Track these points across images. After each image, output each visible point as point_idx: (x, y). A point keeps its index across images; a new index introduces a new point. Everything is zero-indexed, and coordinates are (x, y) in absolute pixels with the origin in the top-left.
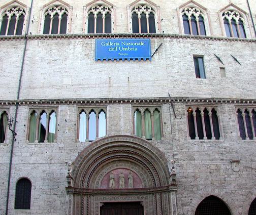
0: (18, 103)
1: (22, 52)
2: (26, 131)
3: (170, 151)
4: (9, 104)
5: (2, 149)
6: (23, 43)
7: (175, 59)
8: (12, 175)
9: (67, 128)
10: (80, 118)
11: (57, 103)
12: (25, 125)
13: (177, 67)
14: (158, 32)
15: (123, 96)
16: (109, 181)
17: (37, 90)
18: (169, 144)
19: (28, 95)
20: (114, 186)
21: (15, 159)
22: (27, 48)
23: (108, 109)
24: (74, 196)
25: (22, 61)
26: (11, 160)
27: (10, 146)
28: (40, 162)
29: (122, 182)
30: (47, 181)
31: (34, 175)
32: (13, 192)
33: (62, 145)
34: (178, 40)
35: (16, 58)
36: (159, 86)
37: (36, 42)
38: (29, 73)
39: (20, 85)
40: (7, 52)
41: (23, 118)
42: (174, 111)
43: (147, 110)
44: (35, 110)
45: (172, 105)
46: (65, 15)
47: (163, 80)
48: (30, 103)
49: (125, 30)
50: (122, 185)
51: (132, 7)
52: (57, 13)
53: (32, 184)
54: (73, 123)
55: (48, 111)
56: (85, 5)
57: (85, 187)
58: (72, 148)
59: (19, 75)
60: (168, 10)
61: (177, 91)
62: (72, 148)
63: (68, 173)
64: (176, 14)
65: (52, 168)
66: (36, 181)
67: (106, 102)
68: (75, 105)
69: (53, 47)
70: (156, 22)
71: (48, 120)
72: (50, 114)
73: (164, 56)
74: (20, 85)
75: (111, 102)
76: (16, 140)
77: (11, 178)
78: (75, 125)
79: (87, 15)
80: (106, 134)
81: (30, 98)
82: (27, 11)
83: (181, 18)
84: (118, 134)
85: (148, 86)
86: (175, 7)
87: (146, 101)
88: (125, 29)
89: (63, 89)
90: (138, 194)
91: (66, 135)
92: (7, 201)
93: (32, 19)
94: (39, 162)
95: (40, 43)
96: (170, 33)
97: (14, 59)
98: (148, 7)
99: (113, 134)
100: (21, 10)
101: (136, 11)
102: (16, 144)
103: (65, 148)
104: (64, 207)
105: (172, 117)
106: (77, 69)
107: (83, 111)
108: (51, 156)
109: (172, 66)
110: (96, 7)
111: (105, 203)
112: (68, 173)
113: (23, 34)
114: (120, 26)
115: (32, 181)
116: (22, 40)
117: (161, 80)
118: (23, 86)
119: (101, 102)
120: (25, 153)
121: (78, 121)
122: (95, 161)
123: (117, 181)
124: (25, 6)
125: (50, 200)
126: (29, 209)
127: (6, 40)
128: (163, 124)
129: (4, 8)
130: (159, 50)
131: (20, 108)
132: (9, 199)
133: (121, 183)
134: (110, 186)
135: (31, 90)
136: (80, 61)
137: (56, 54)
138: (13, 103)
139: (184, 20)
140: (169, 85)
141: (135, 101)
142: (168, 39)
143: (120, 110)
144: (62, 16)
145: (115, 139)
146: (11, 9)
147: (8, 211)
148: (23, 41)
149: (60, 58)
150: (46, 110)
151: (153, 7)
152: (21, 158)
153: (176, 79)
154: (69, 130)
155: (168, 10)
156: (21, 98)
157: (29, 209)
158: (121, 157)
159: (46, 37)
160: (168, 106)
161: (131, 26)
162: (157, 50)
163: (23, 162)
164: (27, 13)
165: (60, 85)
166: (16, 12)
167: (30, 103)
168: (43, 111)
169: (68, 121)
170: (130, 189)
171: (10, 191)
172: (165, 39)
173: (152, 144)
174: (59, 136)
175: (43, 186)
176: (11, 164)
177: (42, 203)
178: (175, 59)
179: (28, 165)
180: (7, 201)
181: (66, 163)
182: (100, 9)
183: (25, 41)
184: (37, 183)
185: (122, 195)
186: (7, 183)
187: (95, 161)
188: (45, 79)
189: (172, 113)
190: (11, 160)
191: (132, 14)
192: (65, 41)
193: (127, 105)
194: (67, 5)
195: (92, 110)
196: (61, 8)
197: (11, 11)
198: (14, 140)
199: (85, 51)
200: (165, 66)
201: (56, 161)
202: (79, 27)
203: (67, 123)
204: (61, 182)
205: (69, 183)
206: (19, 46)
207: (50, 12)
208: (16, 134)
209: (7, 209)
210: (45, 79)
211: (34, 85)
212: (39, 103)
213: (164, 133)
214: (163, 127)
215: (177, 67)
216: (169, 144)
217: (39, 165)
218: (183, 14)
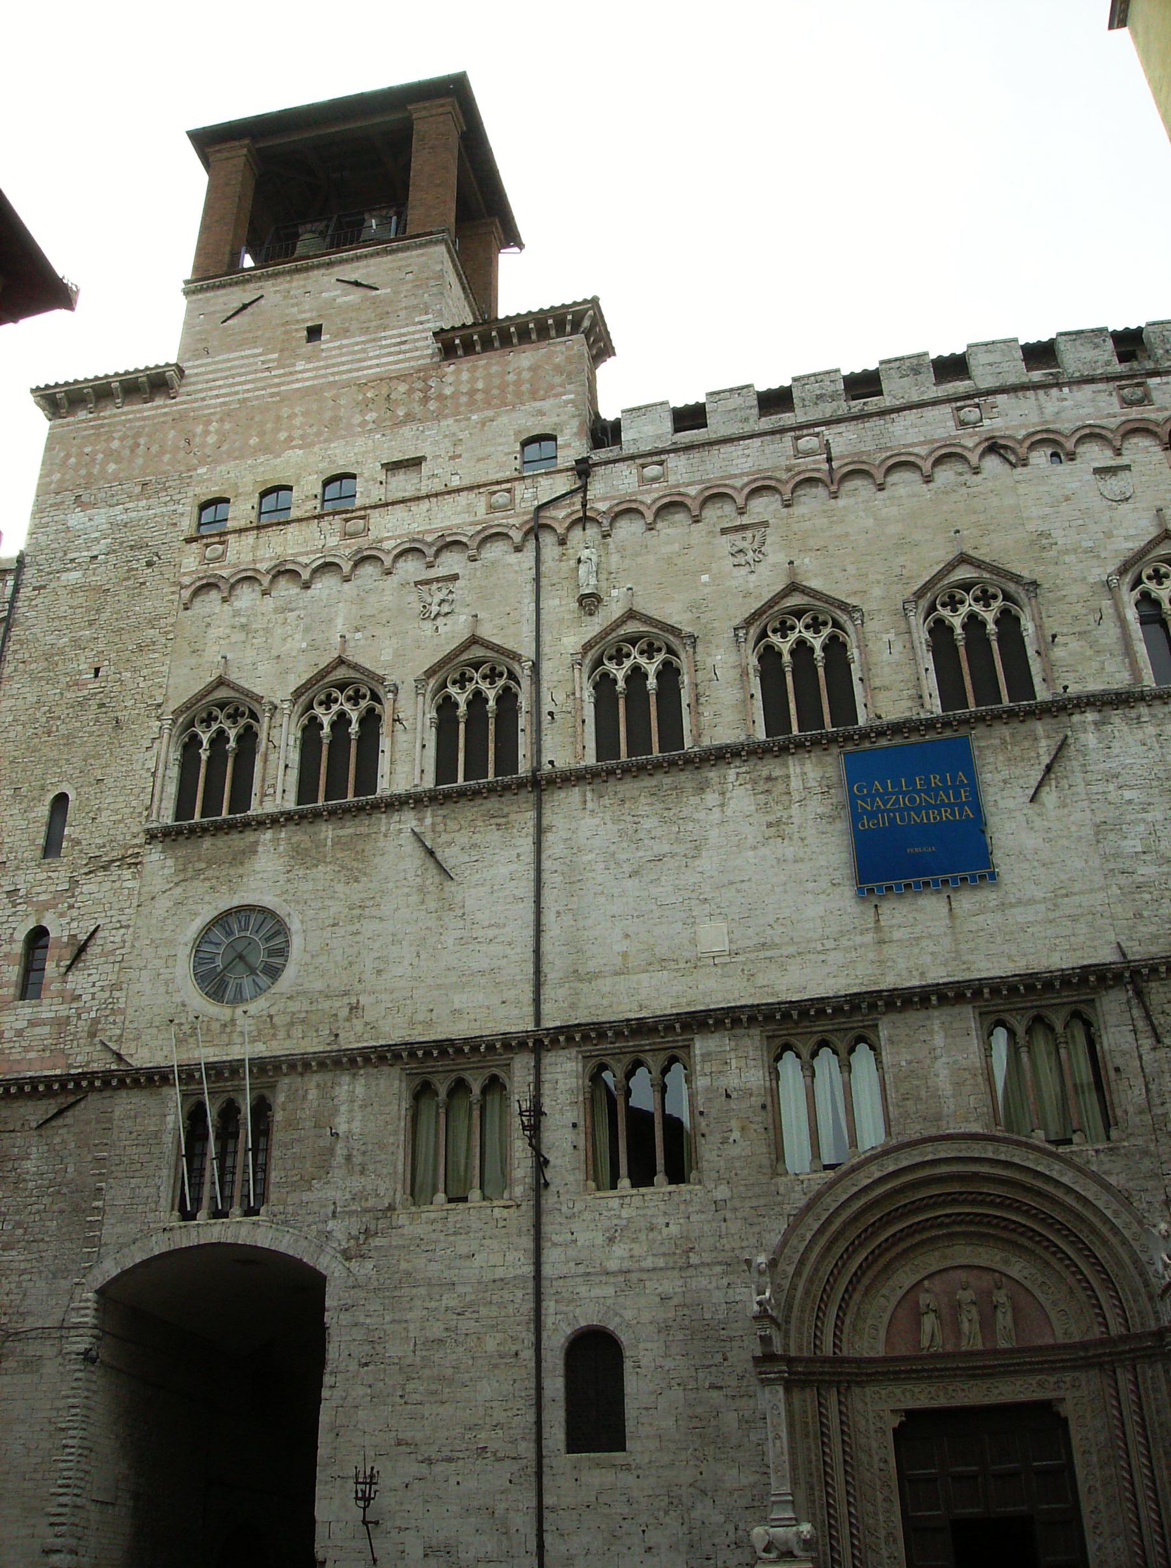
0: (539, 1042)
1: (530, 840)
2: (581, 1144)
3: (1150, 1184)
4: (507, 1046)
5: (501, 1223)
6: (529, 806)
7: (1128, 794)
8: (549, 1321)
9: (734, 1124)
10: (813, 1075)
11: (686, 1027)
12: (575, 1125)
13: (1141, 828)
14: (1042, 693)
15: (938, 975)
16: (919, 1324)
17: (605, 985)
18: (1145, 1153)
19: (573, 1006)
20: (939, 1340)
21: (553, 1259)
22: (545, 822)
23: (884, 1033)
24: (787, 1390)
25: (532, 875)
26: (538, 1264)
27: (527, 1207)
28: (648, 1263)
29: (969, 1323)
30: (680, 1336)
31: (629, 1314)
32: (555, 1385)
33: (722, 1192)
34: (1133, 713)
35: (513, 867)
36: (1074, 919)
37: (572, 796)
38: (567, 919)
39: (538, 971)
40: (474, 846)
41: (564, 1098)
42: (1148, 1017)
43: (1039, 1020)
44: (608, 1060)
45: (1139, 994)
46: (669, 673)
47: (1092, 891)
48: (586, 1038)
49: (910, 704)
50: (972, 1338)
51: (924, 604)
52: (636, 669)
53: (627, 1353)
54: (756, 1101)
55: (655, 1062)
56: (737, 622)
57: (828, 1350)
58: (762, 1201)
59: (531, 932)
60: (1076, 590)
61: (1153, 929)
62: (762, 1201)
63: (760, 1303)
64: (1106, 604)
65: (693, 1284)
66: (638, 1341)
67: (873, 1007)
68: (755, 1031)
69: (643, 809)
70: (1031, 652)
71: (658, 1096)
72: (665, 1071)
73: (1081, 789)
74: (538, 971)
75: (292, 1066)
76: (547, 1185)
77: (544, 1335)
78: (764, 1107)
79: (753, 661)
80: (888, 1133)
81: (582, 1016)
82: (524, 673)
83: (1131, 614)
84: (933, 1132)
85: (1030, 924)
86: (1099, 572)
87: (1030, 988)
88: (911, 697)
89: (703, 970)
90: (1041, 1371)
91: (735, 1151)
92: (539, 1423)
93: (547, 707)
94: (644, 1264)
95: (589, 795)
96: (1094, 686)
97: (504, 870)
98: (991, 590)
99: (914, 1130)
100: (501, 675)
101: (945, 612)
102: (549, 1200)
103: (737, 1203)
104: (754, 1437)
105: (1147, 1043)
106: (744, 886)
107: (787, 1047)
108: (688, 1238)
109: (1116, 826)
110: (783, 623)
111: (909, 1413)
112: (760, 1303)
113: (524, 767)
114: (887, 689)
115: (624, 1338)
116: (523, 794)
117: (1082, 893)
118: (552, 974)
119: (855, 1008)
120: (588, 1236)
121: (774, 1093)
122: (849, 1253)
123: (951, 1317)
124: (516, 657)
125: (699, 1410)
126: (622, 1448)
127: (463, 801)
128: (1112, 1073)
129: (435, 672)
130: (1056, 768)
131: (548, 1059)
132: (546, 1416)
133: (966, 1326)
134: (925, 1342)
135: (584, 986)
136: (751, 853)
137: (657, 832)
138: (522, 1045)
139: (1144, 621)
140: (1118, 909)
141: (986, 991)
142: (1090, 716)
143: (931, 1033)
144: (659, 675)
145: (803, 1237)
146: (463, 674)
147: (545, 1461)
148: (527, 797)
149: (676, 848)
150: (648, 1058)
151: (1011, 587)
152: (572, 1253)
153: (1141, 879)
154: (743, 1129)
155: (1076, 590)
156: (547, 1023)
157: (622, 1448)
158: (954, 1223)
159: (611, 772)
160: (1123, 997)
161: (931, 683)
162: (1049, 768)
163: (581, 1269)
164: (525, 683)
165: (687, 955)
166: (484, 686)
167: (586, 1038)
168: (638, 1063)
169: (734, 1095)
170: (1005, 1351)
171: (547, 1383)
172: (1076, 718)
173: (1077, 1159)
174: (707, 1156)
175: (666, 1356)
176: (538, 1277)
177: (671, 1422)
178: (1128, 794)
179: (604, 1278)
180: (539, 1423)
181: (748, 1262)
182: (800, 630)
183: (532, 797)
184: (641, 1346)
185: (973, 1376)
186: (528, 1354)
187: (849, 1253)
188: (627, 936)
189: (1141, 1024)
190: (538, 1264)
191: (930, 632)
192: (685, 778)
193: (957, 1009)
194: (674, 631)
195: (823, 1043)
196: (650, 645)
197: (462, 681)
198: (540, 1185)
199: (765, 808)
200: (1089, 831)
201: (707, 1257)
202: (730, 716)
203: (733, 1104)
204: (731, 1339)
205: (766, 1340)
206: (513, 817)
207: (610, 666)
208: (547, 1162)
209: (540, 1457)
210: (627, 936)
211: (592, 966)
212: (619, 1034)
213: (1119, 1112)
214: (1113, 1084)
215: (1141, 828)
216: (1145, 1153)
217: (645, 1276)
218: (1136, 594)
